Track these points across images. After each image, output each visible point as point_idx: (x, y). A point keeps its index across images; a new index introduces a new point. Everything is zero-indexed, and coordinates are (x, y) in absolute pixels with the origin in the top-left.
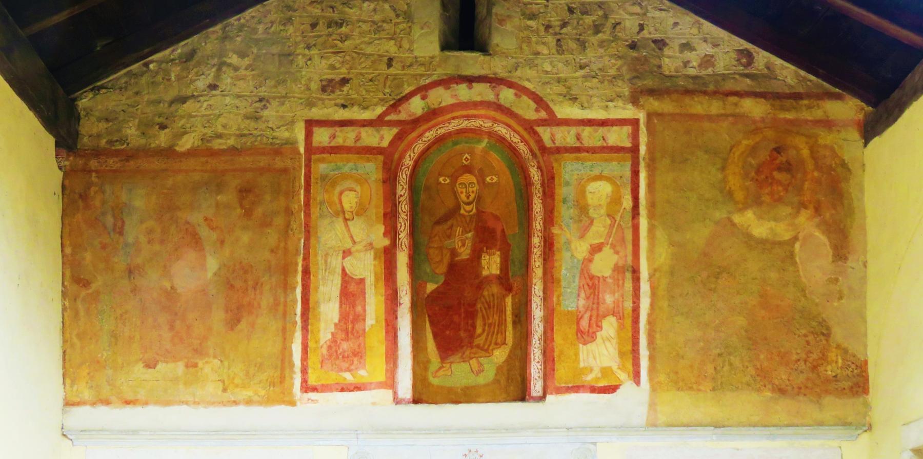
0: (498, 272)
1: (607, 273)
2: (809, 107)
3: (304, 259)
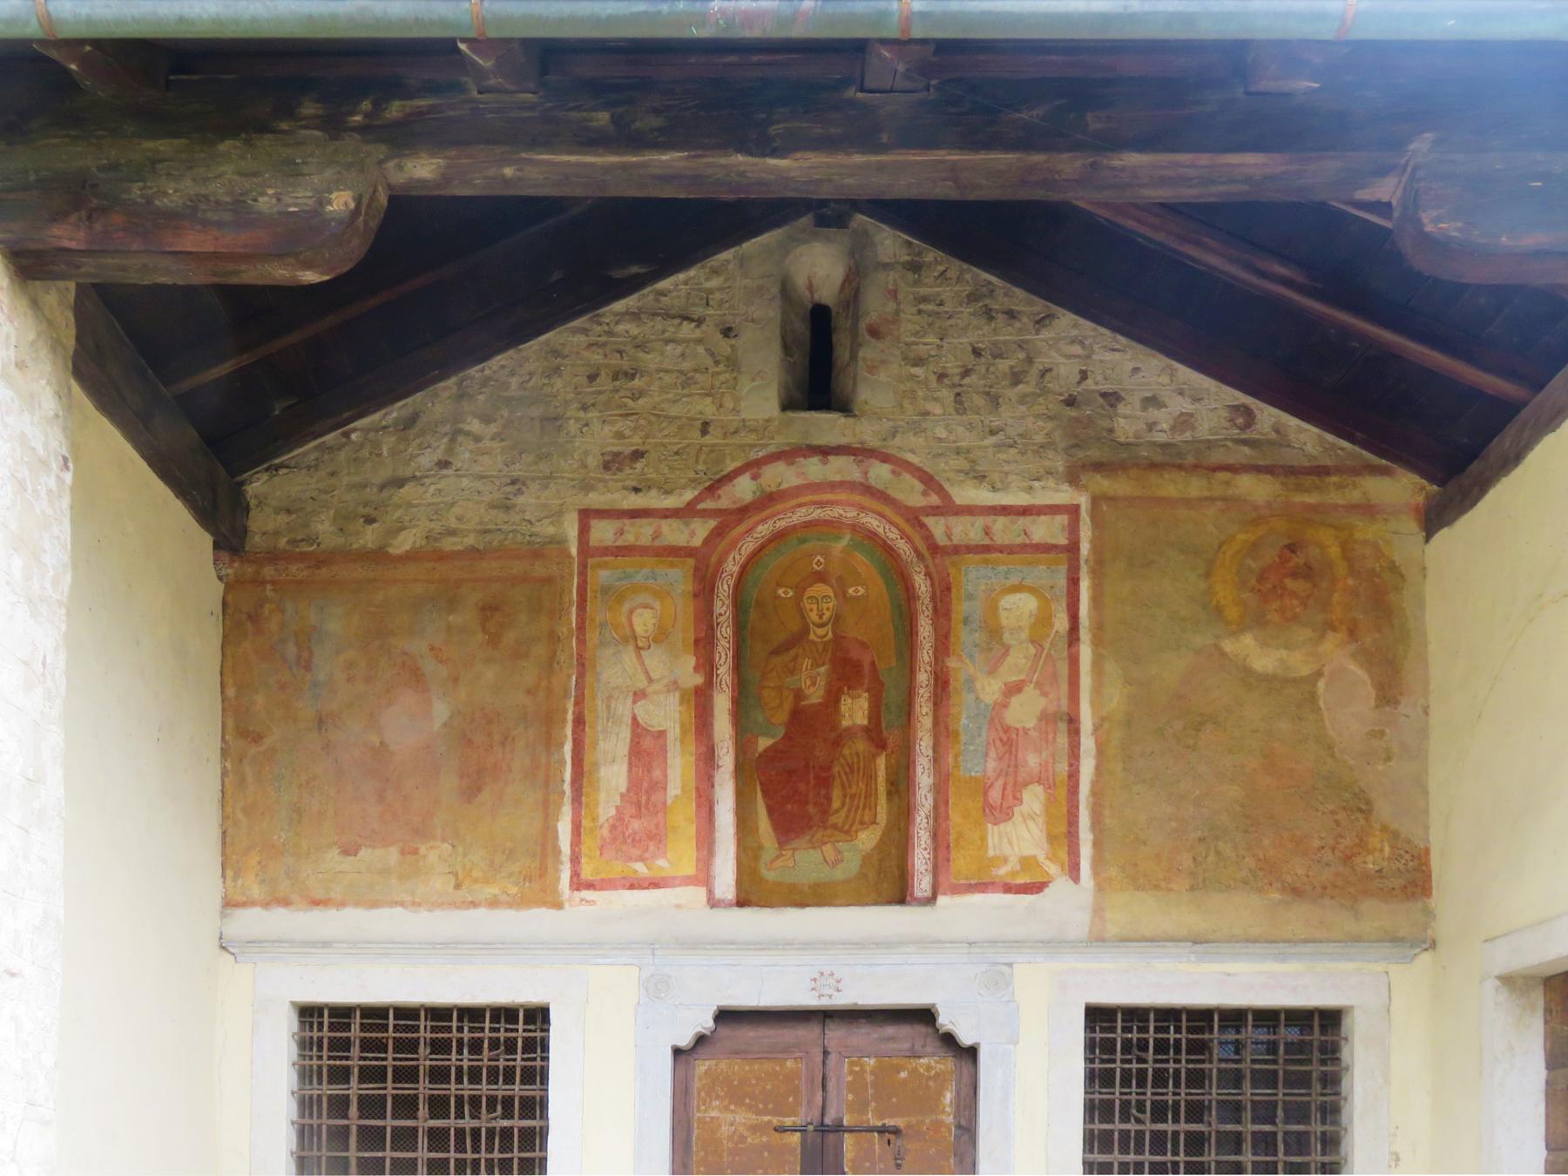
0: (865, 722)
1: (1031, 723)
3: (577, 704)
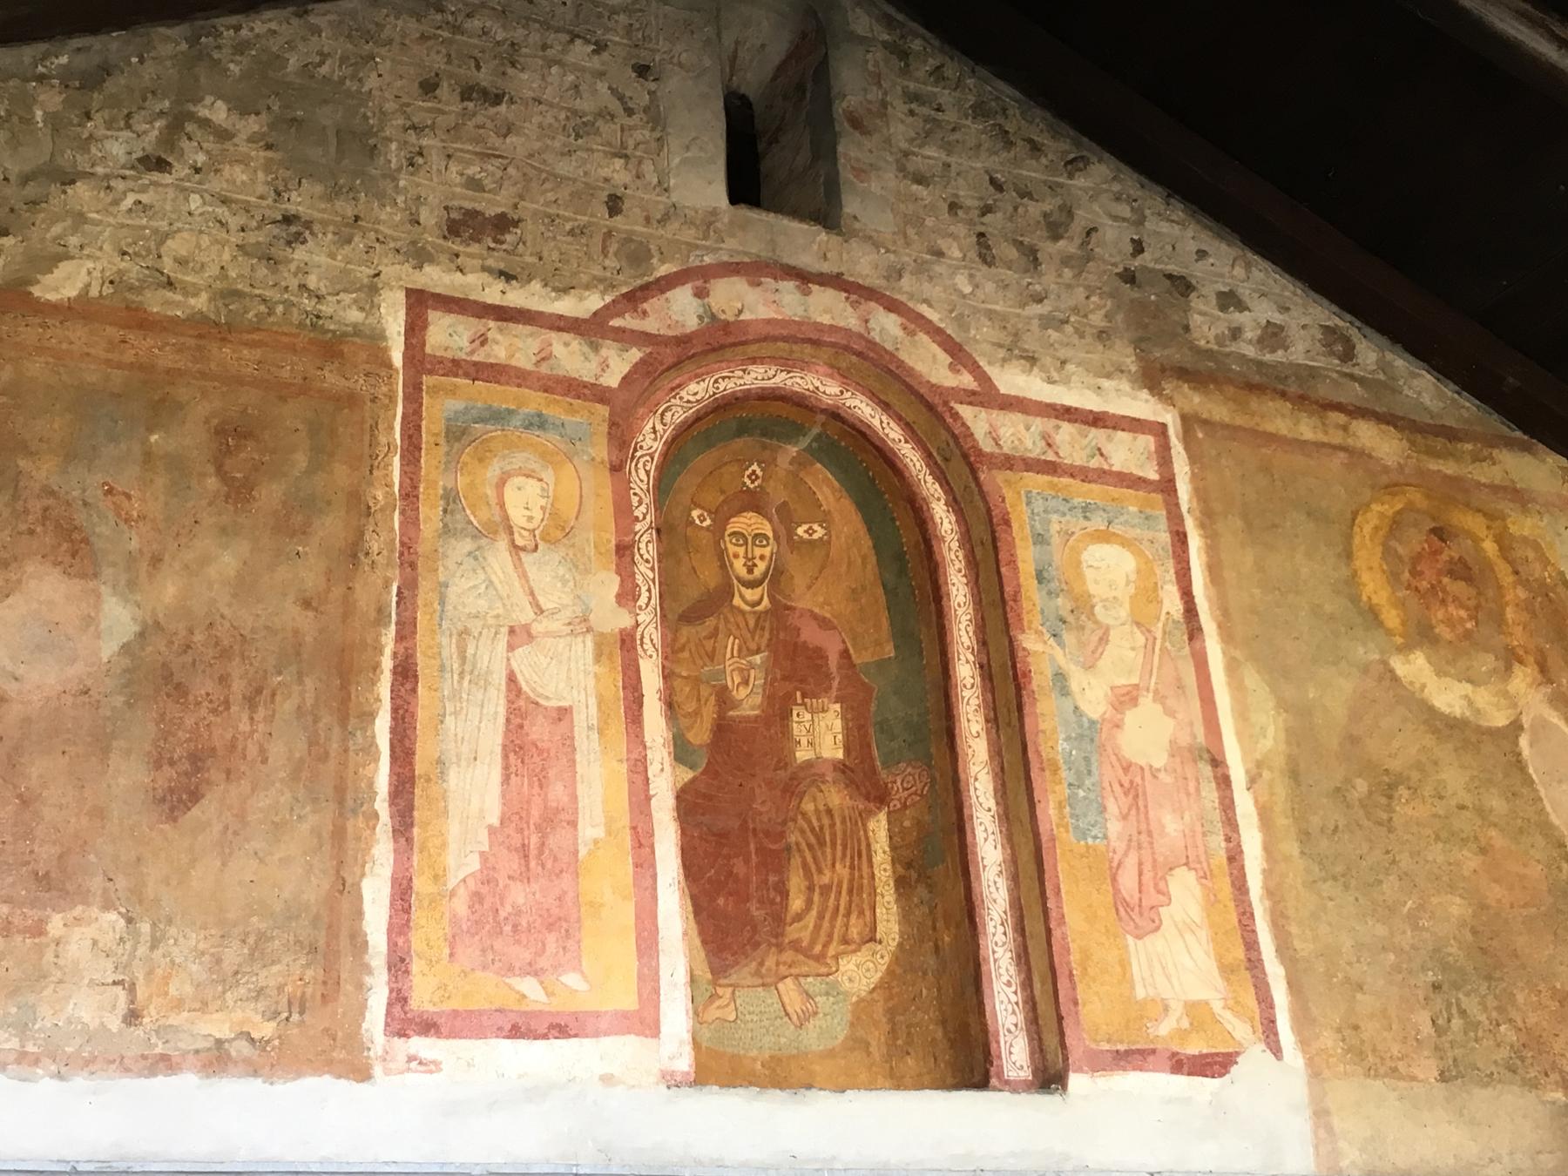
0: (840, 755)
1: (1160, 760)
2: (1477, 458)
3: (400, 638)
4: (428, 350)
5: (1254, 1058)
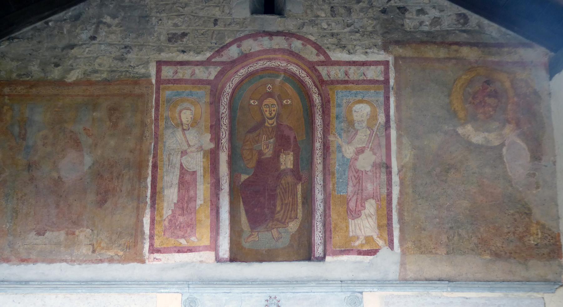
1: (369, 168)
3: (154, 157)
4: (162, 78)
5: (384, 251)
